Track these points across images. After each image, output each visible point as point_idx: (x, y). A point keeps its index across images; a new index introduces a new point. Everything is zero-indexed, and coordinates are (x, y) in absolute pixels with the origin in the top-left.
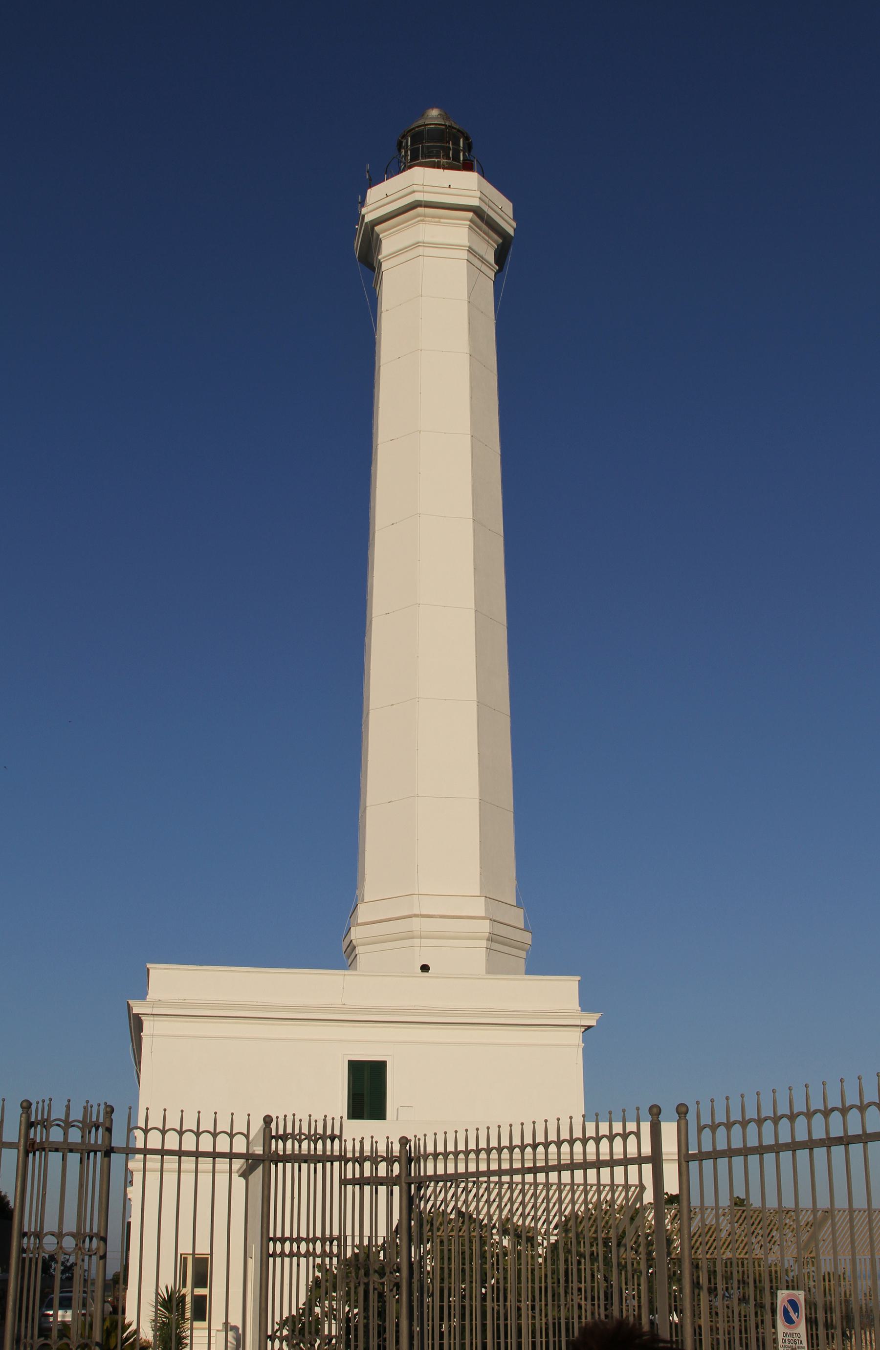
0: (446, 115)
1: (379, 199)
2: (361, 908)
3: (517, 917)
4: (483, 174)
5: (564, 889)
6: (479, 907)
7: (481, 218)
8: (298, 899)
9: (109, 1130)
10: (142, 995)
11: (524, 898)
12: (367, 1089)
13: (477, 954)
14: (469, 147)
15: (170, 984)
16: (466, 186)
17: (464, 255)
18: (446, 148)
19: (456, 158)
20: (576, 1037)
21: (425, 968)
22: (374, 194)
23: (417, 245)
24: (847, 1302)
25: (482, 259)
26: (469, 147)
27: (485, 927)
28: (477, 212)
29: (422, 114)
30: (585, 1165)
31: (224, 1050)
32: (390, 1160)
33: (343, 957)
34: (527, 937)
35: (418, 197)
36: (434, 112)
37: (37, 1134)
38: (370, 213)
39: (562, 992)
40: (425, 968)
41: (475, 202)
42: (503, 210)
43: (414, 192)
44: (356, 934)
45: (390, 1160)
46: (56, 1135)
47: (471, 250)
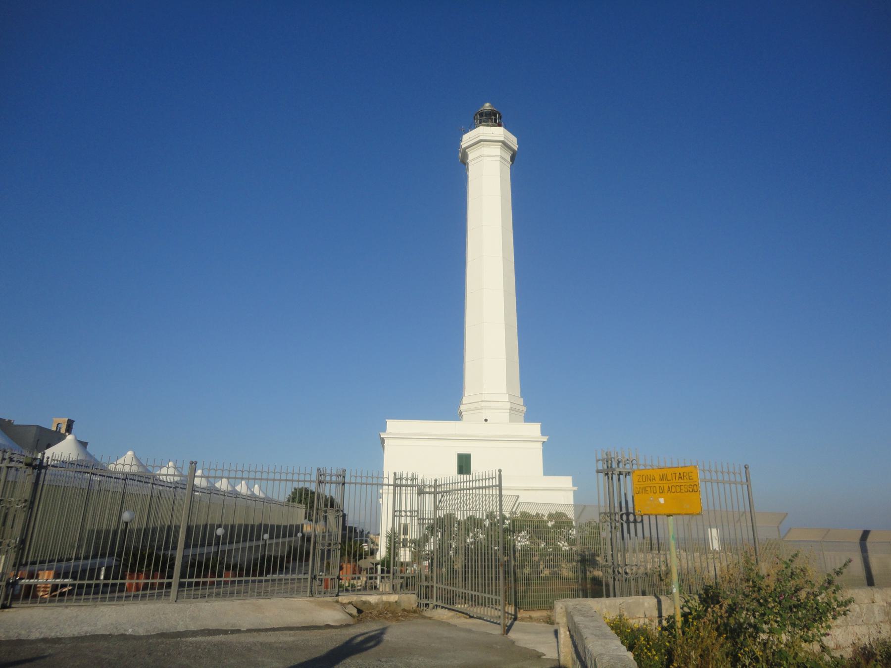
0: (492, 105)
1: (467, 139)
2: (464, 398)
3: (521, 401)
4: (506, 128)
5: (541, 387)
6: (506, 398)
7: (505, 144)
8: (441, 393)
9: (344, 477)
10: (384, 430)
11: (523, 394)
12: (464, 464)
13: (506, 415)
14: (500, 117)
15: (394, 426)
16: (499, 132)
17: (499, 159)
18: (492, 118)
19: (495, 121)
20: (540, 445)
21: (486, 420)
22: (466, 137)
23: (481, 156)
24: (850, 602)
25: (505, 160)
26: (500, 117)
27: (508, 405)
28: (504, 143)
29: (483, 105)
30: (473, 489)
31: (415, 452)
32: (430, 486)
33: (457, 416)
34: (524, 409)
35: (481, 138)
36: (487, 105)
37: (322, 478)
38: (464, 144)
39: (535, 429)
40: (486, 420)
41: (502, 139)
42: (513, 141)
43: (481, 156)
44: (462, 408)
45: (337, 476)
46: (328, 478)
47: (501, 157)
